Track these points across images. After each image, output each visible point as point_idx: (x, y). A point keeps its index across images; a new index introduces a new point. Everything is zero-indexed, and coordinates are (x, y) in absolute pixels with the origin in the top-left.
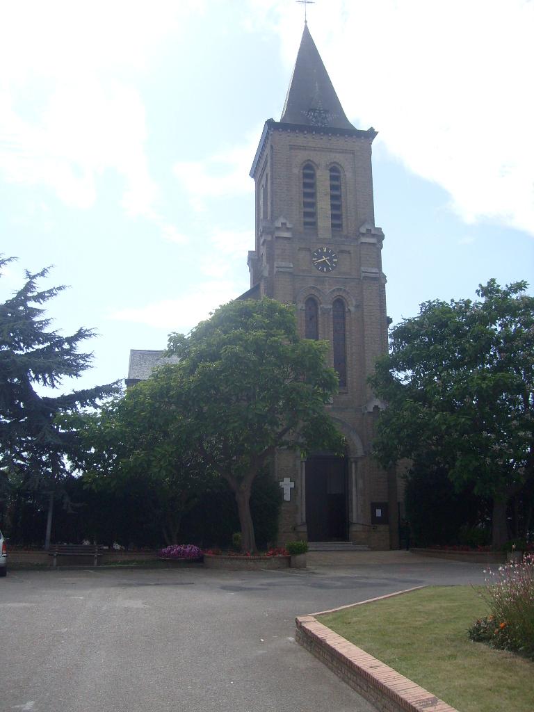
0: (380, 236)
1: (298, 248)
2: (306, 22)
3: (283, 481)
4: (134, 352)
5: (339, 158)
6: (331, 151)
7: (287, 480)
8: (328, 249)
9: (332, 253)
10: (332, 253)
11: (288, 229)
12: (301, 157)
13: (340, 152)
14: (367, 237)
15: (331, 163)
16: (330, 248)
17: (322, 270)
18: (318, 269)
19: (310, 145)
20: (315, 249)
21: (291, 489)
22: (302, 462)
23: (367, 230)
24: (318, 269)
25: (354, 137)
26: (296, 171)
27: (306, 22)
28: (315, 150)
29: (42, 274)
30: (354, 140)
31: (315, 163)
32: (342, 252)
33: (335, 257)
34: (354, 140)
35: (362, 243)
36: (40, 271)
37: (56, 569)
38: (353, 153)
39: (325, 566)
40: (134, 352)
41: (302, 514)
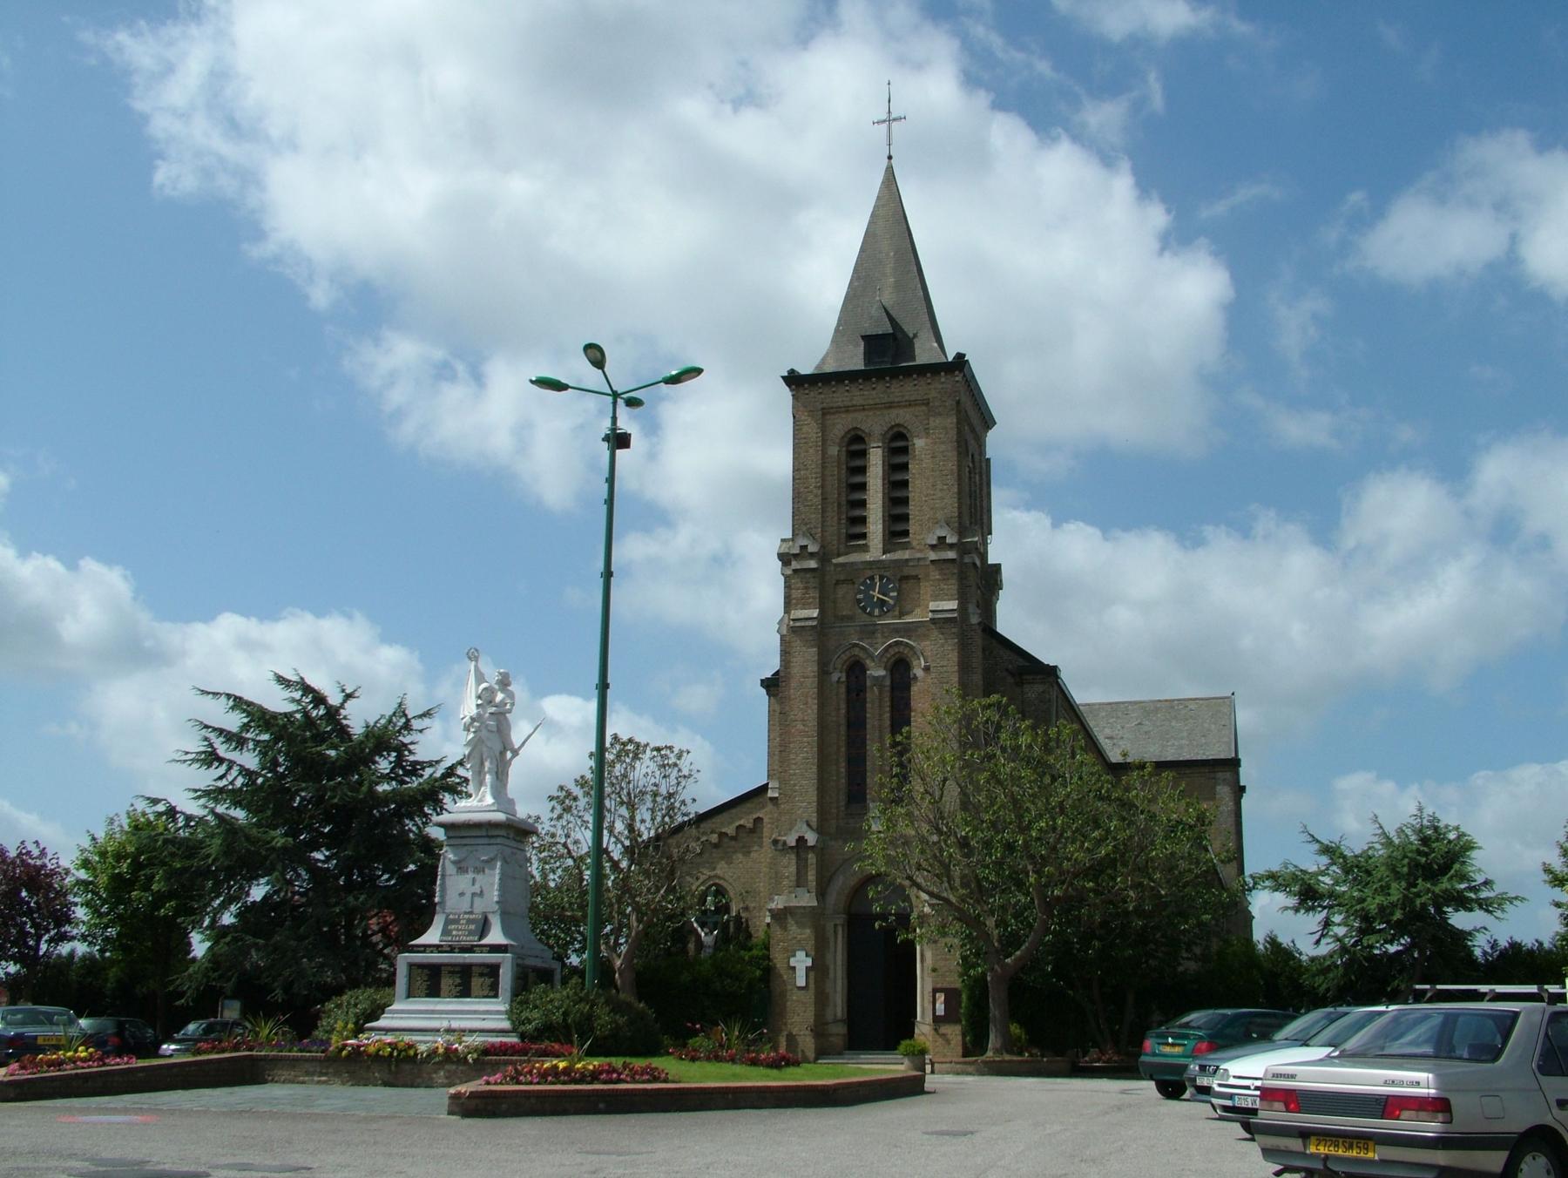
1: (834, 582)
2: (890, 158)
3: (794, 956)
4: (1000, 565)
5: (902, 416)
7: (801, 955)
11: (812, 555)
12: (840, 425)
13: (905, 406)
15: (892, 427)
16: (885, 574)
20: (862, 580)
21: (807, 968)
22: (836, 925)
23: (939, 538)
27: (890, 158)
28: (864, 409)
30: (929, 381)
34: (929, 381)
36: (420, 728)
37: (1331, 957)
40: (1000, 565)
41: (835, 1006)
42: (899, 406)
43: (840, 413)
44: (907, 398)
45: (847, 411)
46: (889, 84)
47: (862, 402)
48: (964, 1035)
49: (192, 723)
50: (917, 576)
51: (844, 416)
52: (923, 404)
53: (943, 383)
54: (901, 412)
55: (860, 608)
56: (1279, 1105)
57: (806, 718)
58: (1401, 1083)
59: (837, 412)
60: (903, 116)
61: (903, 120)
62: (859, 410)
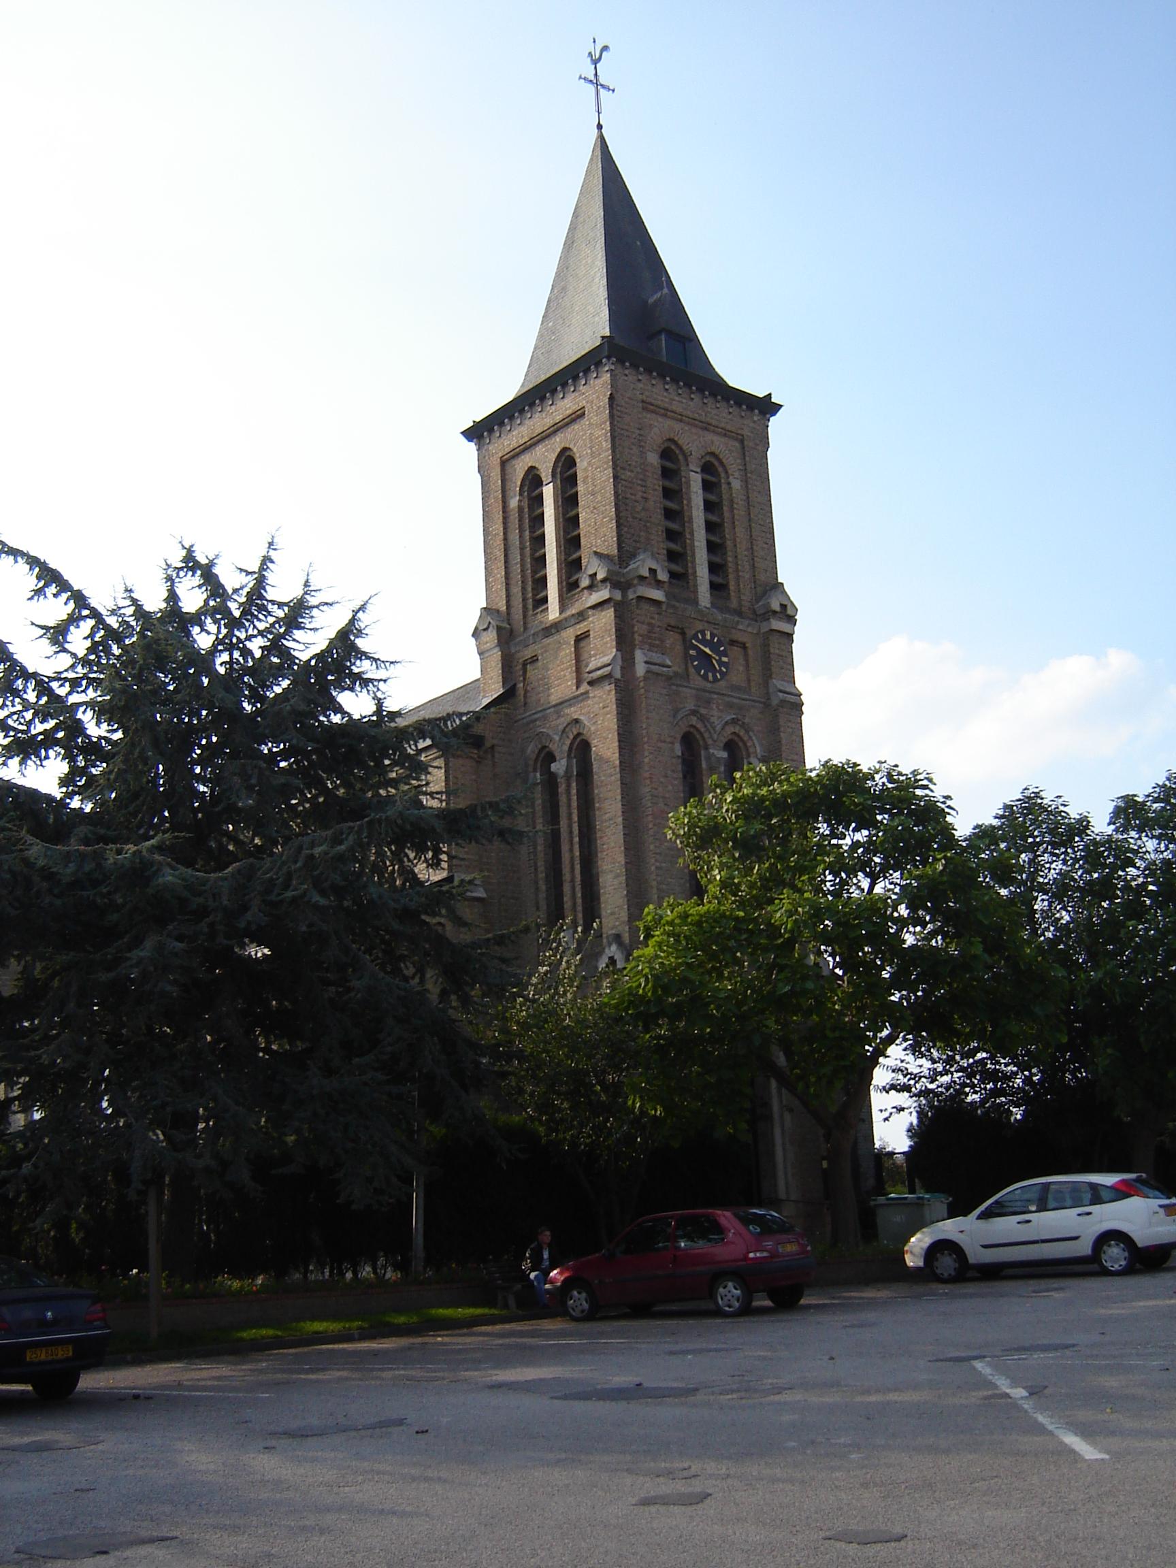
0: (788, 614)
2: (600, 127)
5: (719, 445)
6: (706, 429)
8: (713, 635)
9: (720, 643)
10: (720, 643)
14: (780, 619)
17: (705, 677)
18: (699, 674)
19: (674, 408)
24: (699, 674)
25: (756, 411)
26: (653, 459)
27: (600, 127)
29: (385, 681)
31: (681, 449)
32: (733, 642)
33: (725, 654)
34: (654, 382)
35: (640, 598)
38: (742, 442)
39: (320, 1433)
42: (713, 431)
43: (657, 414)
44: (722, 425)
45: (665, 415)
46: (594, 42)
47: (680, 410)
48: (161, 611)
49: (25, 772)
50: (744, 644)
51: (660, 419)
52: (736, 439)
53: (754, 422)
54: (715, 438)
55: (721, 679)
56: (976, 1255)
57: (667, 795)
58: (572, 859)
59: (653, 412)
60: (611, 88)
61: (611, 92)
62: (718, 434)
